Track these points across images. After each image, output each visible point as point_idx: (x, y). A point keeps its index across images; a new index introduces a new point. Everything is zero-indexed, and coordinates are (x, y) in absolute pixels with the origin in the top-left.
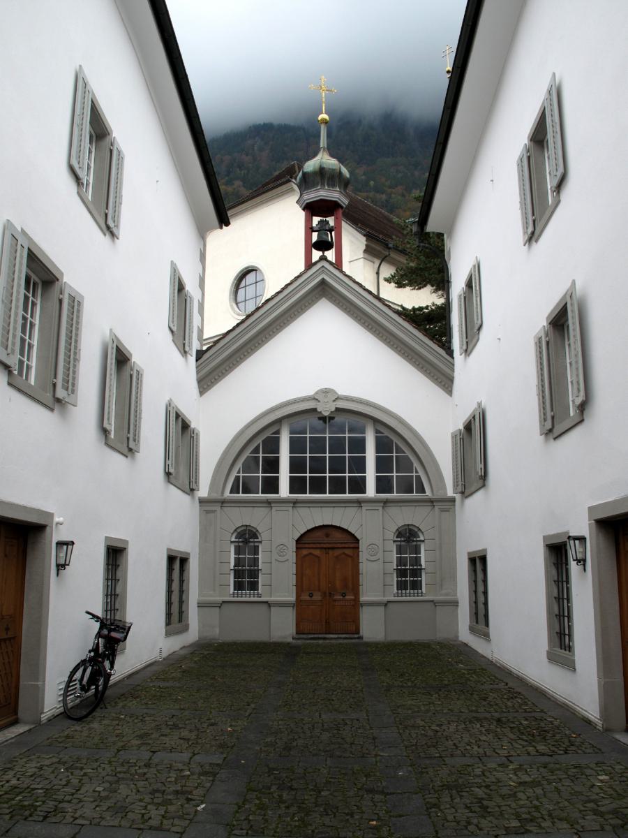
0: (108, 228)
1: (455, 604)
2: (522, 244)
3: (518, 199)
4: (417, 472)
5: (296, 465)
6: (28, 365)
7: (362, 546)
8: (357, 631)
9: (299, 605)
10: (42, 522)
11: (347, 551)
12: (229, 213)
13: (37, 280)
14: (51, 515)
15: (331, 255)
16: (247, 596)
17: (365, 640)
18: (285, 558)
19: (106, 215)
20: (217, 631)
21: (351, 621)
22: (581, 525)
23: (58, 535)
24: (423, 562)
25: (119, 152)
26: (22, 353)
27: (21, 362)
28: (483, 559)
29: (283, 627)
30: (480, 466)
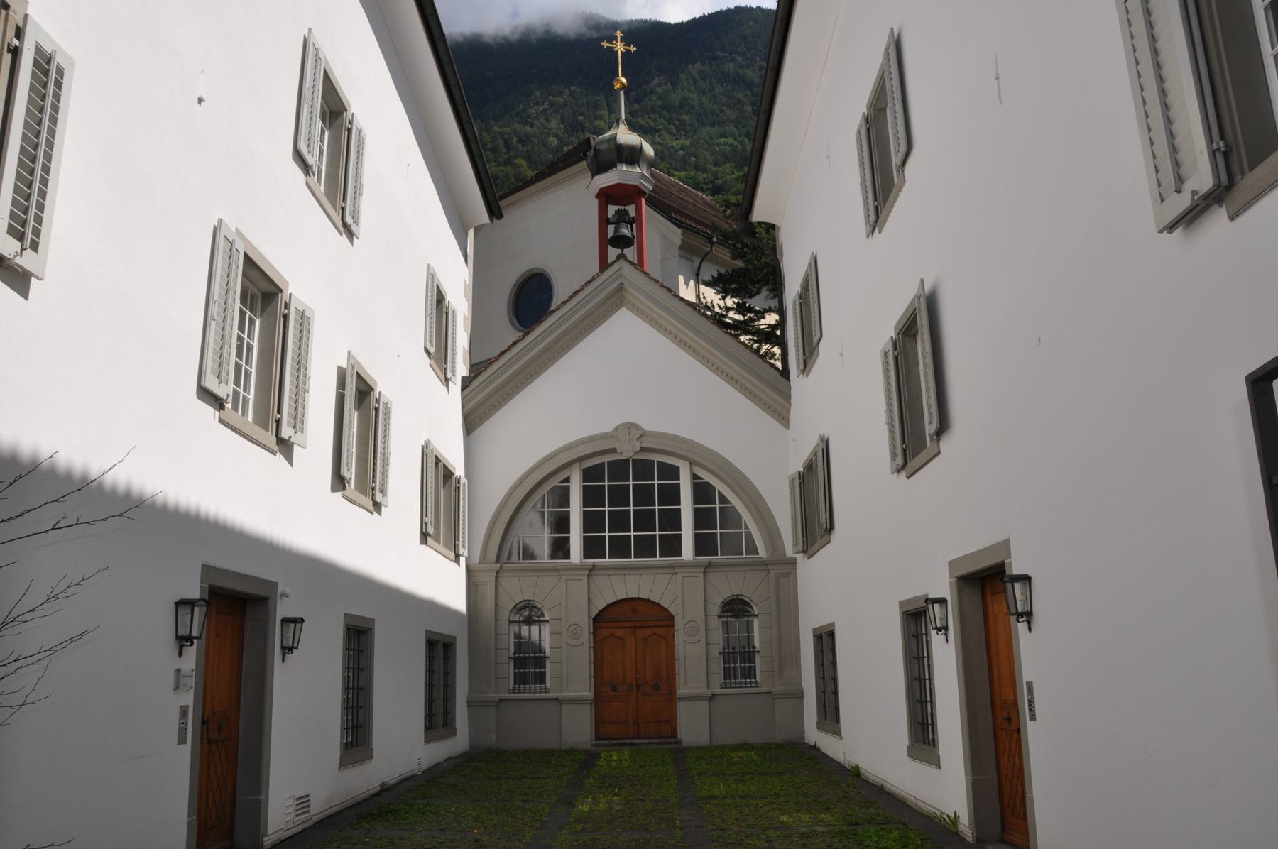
0: (345, 225)
1: (799, 695)
2: (865, 235)
3: (859, 181)
4: (746, 527)
5: (591, 522)
6: (246, 370)
7: (678, 623)
8: (674, 735)
9: (599, 701)
10: (262, 593)
11: (658, 630)
12: (502, 204)
13: (256, 291)
14: (275, 585)
15: (631, 253)
16: (531, 691)
17: (684, 744)
18: (579, 642)
19: (343, 209)
20: (494, 737)
21: (666, 727)
22: (942, 587)
23: (283, 610)
24: (757, 643)
25: (360, 132)
26: (237, 383)
27: (236, 394)
28: (831, 635)
29: (578, 728)
30: (824, 517)
